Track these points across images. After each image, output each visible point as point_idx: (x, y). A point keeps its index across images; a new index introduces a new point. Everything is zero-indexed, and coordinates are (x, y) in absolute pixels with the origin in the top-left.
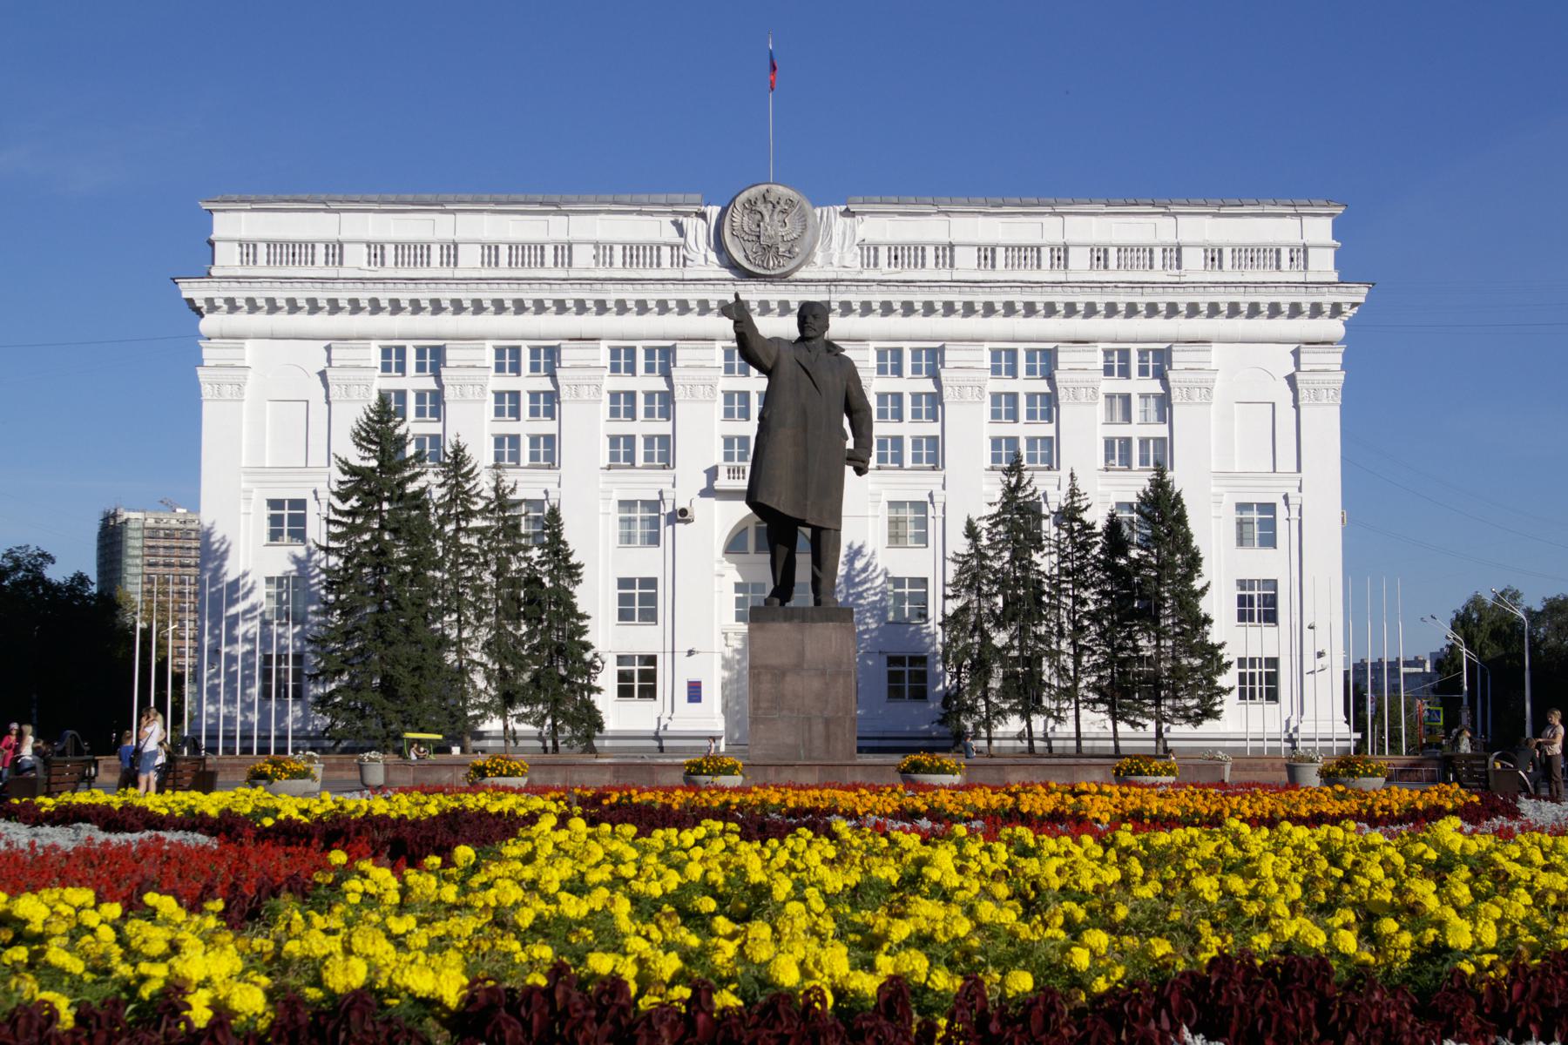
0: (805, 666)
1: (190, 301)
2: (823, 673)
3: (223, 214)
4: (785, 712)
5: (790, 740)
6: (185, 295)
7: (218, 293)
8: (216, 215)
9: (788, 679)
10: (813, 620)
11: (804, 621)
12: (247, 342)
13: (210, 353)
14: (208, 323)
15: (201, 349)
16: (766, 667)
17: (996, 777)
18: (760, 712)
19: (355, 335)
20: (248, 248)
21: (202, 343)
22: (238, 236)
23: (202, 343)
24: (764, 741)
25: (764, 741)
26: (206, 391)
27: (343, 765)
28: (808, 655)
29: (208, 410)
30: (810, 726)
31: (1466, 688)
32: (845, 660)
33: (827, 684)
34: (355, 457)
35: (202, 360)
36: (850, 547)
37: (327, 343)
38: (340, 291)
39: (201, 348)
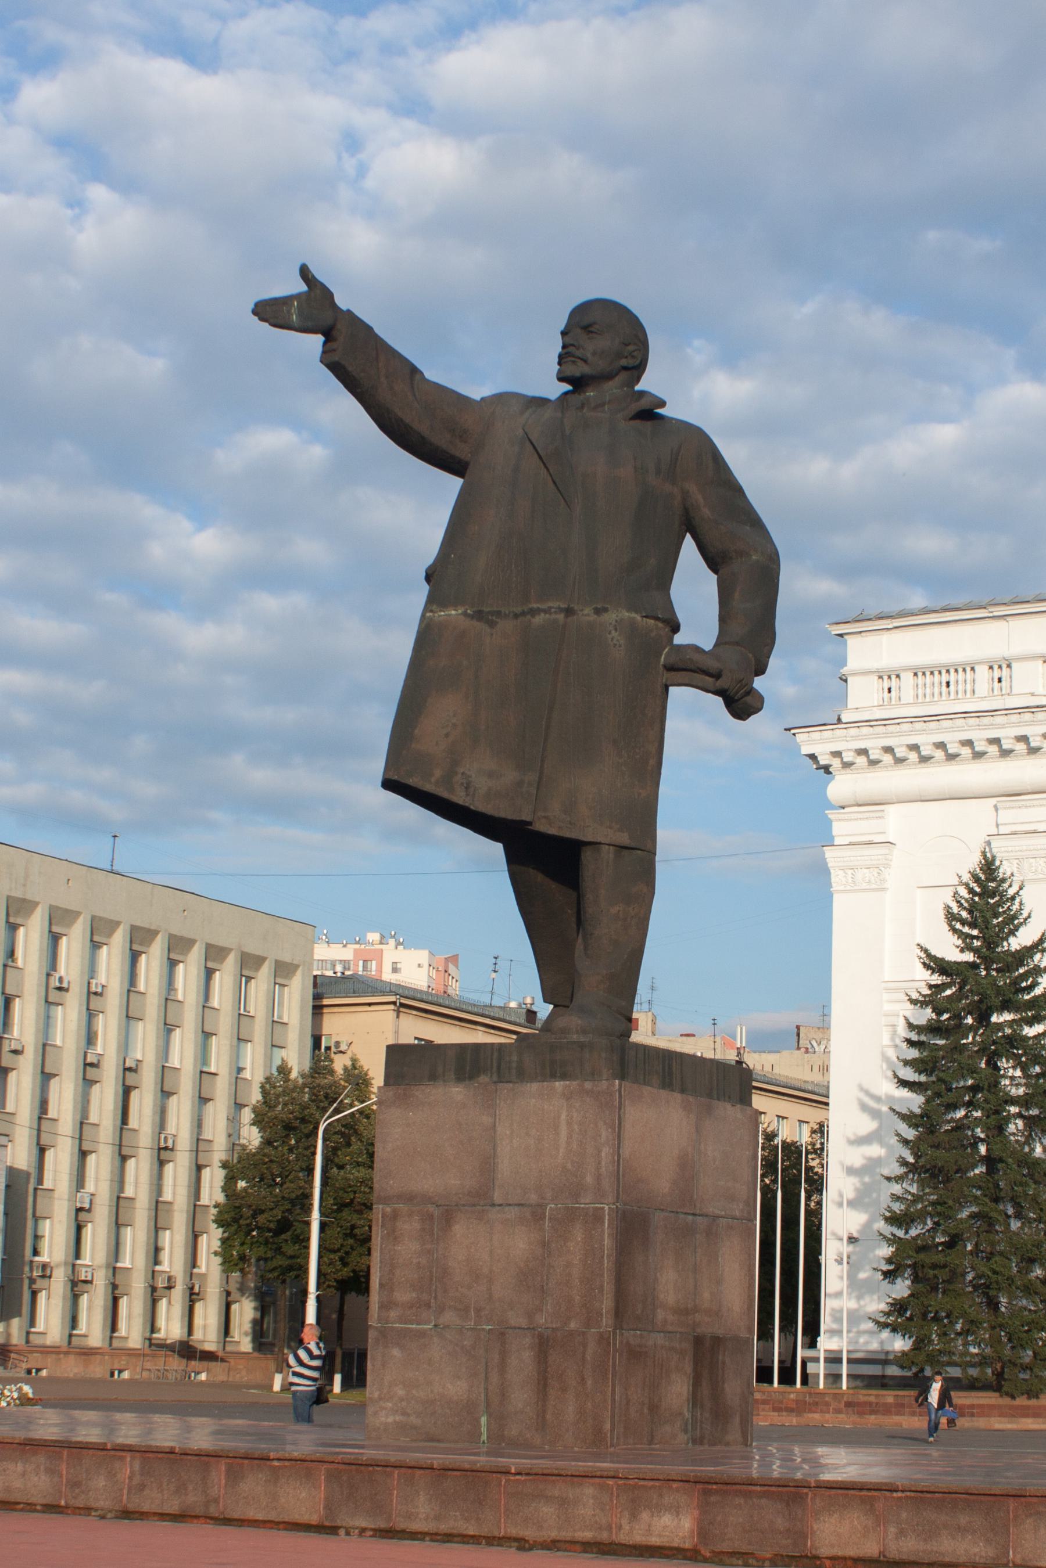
0: (497, 1197)
1: (813, 757)
2: (537, 1214)
3: (857, 638)
4: (449, 1317)
5: (456, 1389)
6: (806, 750)
7: (845, 741)
8: (850, 641)
9: (458, 1229)
10: (522, 1075)
11: (501, 1078)
12: (890, 809)
13: (842, 828)
14: (840, 787)
15: (829, 823)
16: (409, 1198)
17: (781, 1523)
18: (393, 1314)
19: (1029, 789)
20: (888, 675)
21: (832, 814)
22: (875, 665)
23: (832, 814)
24: (401, 1392)
25: (401, 1392)
26: (838, 879)
27: (902, 1405)
28: (505, 1167)
29: (840, 905)
30: (504, 1354)
31: (468, 1068)
32: (589, 1180)
33: (544, 1244)
34: (950, 950)
35: (832, 838)
36: (962, 951)
37: (994, 801)
38: (1002, 726)
39: (830, 822)
